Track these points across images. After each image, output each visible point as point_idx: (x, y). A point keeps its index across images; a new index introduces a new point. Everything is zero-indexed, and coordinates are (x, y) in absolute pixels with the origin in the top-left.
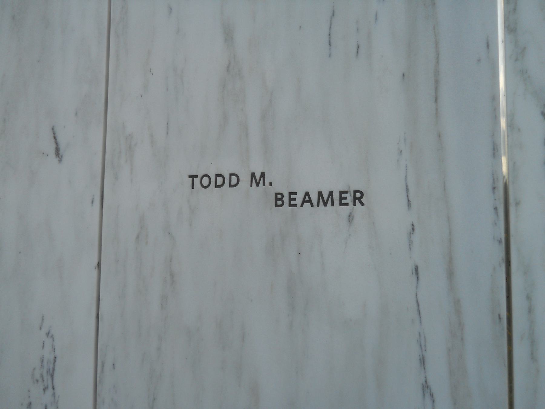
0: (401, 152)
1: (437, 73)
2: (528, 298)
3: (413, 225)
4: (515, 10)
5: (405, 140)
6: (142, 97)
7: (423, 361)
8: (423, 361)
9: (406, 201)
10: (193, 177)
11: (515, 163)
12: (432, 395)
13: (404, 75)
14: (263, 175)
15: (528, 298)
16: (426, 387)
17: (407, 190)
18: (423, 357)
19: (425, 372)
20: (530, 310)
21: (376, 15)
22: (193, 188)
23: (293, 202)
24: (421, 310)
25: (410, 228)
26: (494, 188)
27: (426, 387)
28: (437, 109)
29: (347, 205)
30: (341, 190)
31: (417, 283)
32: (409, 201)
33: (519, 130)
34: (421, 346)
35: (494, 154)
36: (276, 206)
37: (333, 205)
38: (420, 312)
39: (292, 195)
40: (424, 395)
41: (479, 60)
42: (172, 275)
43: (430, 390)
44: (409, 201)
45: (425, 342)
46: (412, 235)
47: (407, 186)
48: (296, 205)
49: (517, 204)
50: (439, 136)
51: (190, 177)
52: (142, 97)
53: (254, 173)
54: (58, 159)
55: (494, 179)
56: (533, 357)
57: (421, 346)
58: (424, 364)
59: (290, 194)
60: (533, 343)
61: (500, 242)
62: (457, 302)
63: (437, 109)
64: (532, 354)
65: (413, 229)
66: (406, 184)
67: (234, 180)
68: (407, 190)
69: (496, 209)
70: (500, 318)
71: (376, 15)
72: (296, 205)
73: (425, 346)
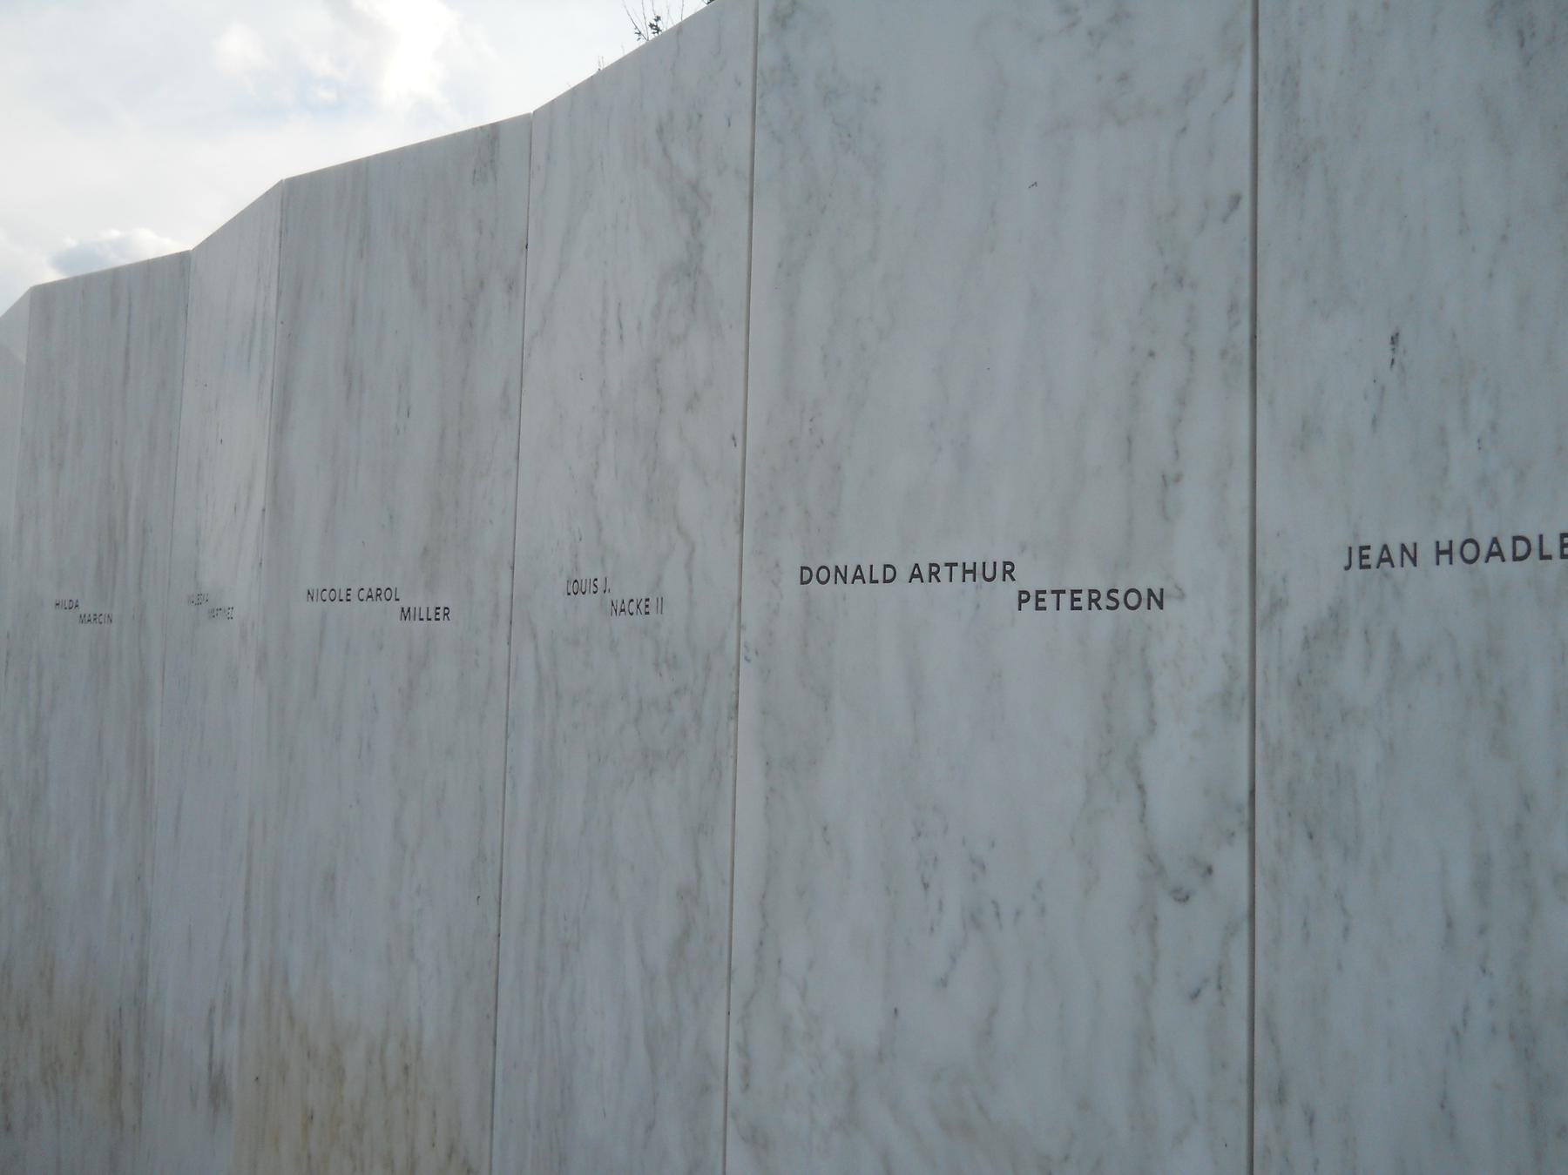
5: (639, 328)
6: (896, 1011)
23: (1365, 562)
29: (1080, 608)
36: (1072, 591)
48: (1369, 567)
52: (896, 1011)
54: (1391, 346)
59: (1362, 548)
67: (890, 572)
72: (1369, 567)
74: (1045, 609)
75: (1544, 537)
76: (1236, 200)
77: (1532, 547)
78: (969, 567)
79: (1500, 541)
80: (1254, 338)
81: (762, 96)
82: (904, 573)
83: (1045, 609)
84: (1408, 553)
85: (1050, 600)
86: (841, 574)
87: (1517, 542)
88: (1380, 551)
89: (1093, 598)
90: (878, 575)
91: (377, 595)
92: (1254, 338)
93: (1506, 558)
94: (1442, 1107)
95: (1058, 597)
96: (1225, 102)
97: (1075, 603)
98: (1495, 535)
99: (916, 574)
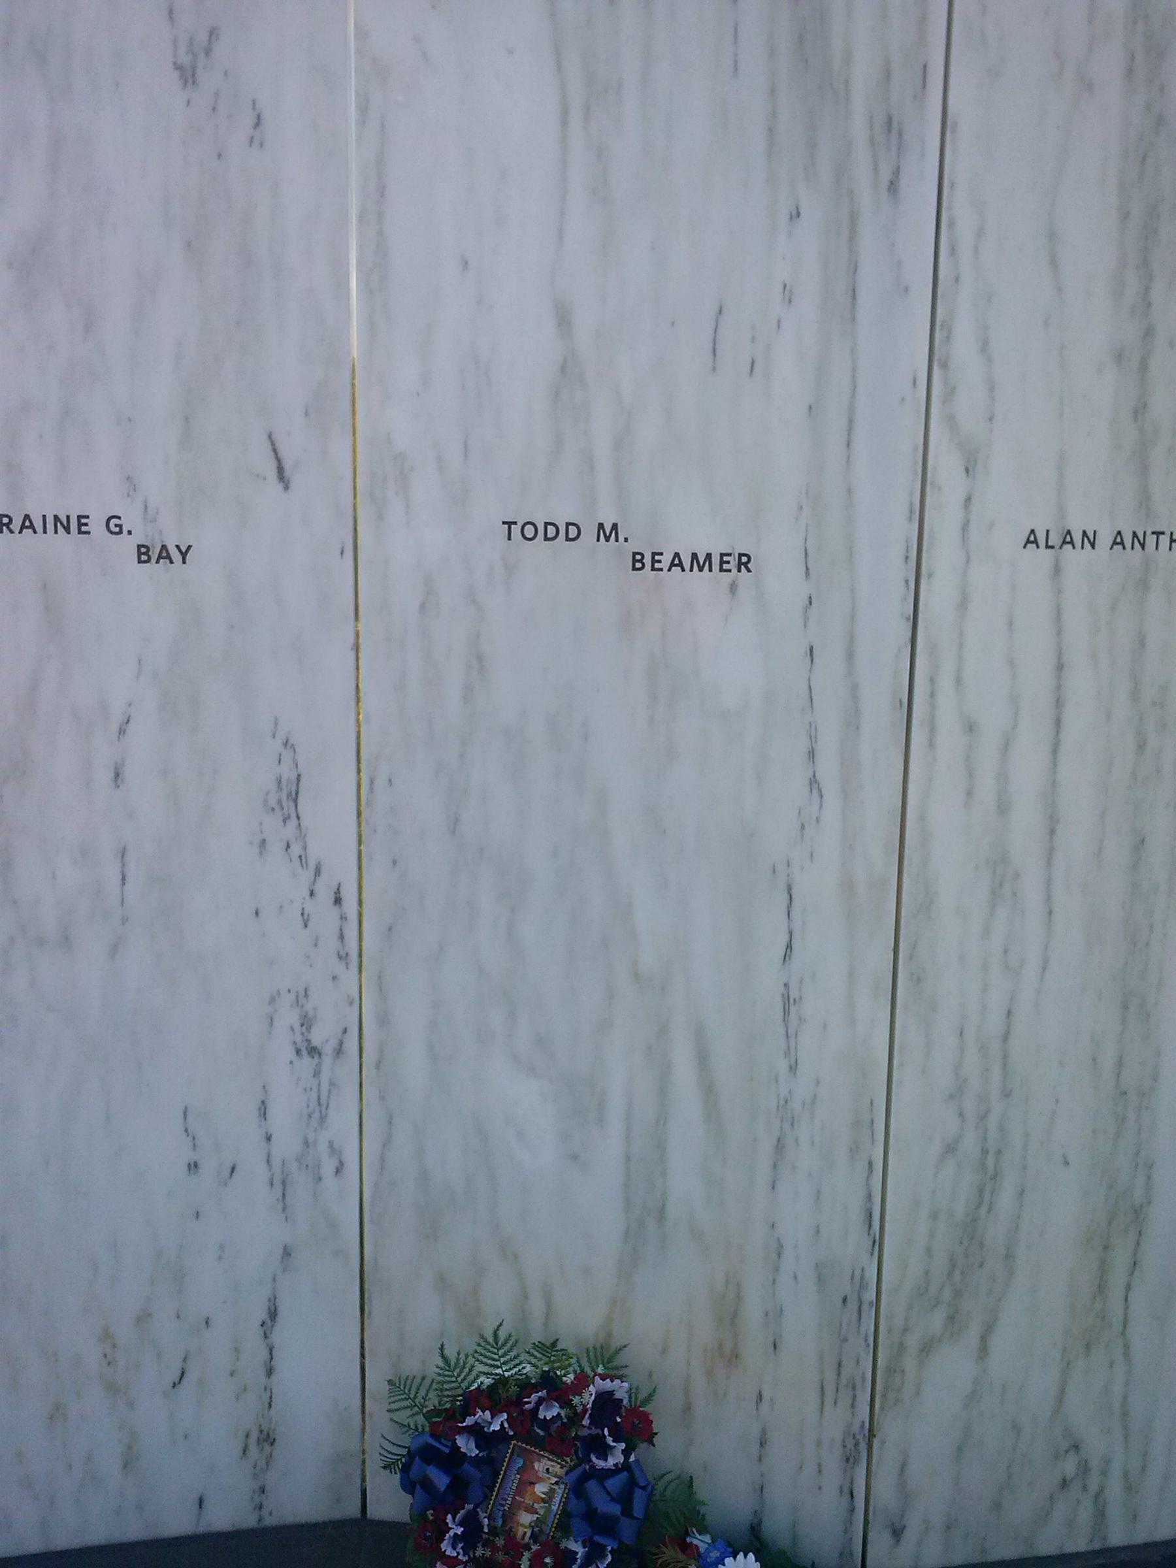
1: (851, 409)
2: (932, 681)
10: (510, 524)
12: (820, 790)
14: (615, 527)
15: (932, 681)
16: (814, 782)
20: (932, 695)
22: (1048, 531)
27: (814, 782)
32: (807, 568)
34: (811, 737)
37: (710, 570)
42: (480, 659)
44: (807, 568)
49: (930, 576)
51: (504, 523)
53: (711, 554)
56: (931, 744)
57: (811, 737)
60: (932, 730)
65: (810, 603)
67: (573, 531)
74: (88, 533)
75: (71, 517)
77: (561, 532)
79: (1122, 533)
82: (1105, 540)
83: (88, 533)
84: (61, 523)
85: (1151, 540)
86: (1088, 539)
88: (1028, 533)
89: (743, 561)
90: (1054, 540)
93: (37, 530)
94: (453, 832)
95: (1057, 570)
98: (1033, 528)
99: (1118, 541)
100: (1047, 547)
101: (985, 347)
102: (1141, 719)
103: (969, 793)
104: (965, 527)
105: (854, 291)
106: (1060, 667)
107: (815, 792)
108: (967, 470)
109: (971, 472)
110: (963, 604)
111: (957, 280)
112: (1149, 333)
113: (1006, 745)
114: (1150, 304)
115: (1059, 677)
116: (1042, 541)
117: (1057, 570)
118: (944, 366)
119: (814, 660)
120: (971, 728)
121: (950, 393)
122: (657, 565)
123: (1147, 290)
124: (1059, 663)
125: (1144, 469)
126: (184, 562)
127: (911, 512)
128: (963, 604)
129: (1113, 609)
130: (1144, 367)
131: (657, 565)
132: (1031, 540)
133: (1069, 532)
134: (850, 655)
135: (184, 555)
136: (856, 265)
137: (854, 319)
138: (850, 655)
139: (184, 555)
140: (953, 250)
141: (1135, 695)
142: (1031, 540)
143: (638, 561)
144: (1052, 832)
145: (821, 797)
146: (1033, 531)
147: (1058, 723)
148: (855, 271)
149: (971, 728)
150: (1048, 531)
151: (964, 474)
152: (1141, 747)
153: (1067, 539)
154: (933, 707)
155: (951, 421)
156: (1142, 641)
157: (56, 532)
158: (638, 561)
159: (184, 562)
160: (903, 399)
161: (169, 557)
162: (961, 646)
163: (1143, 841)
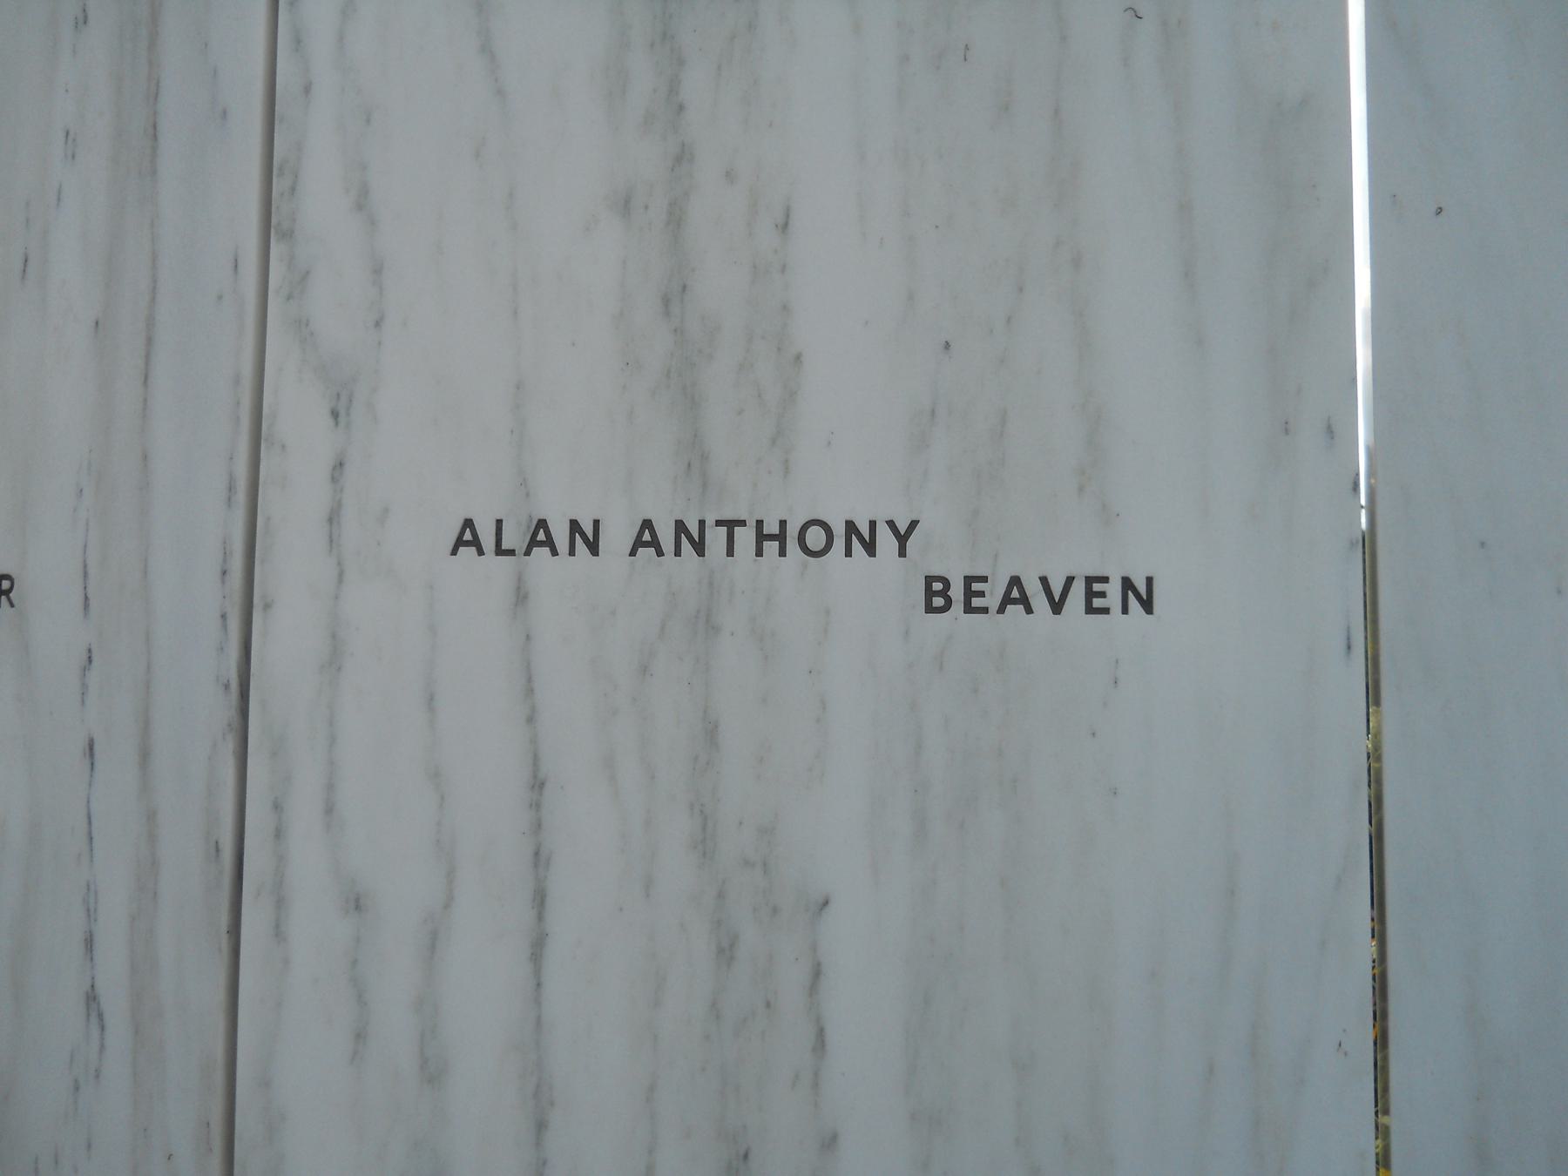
0: (81, 491)
1: (150, 322)
2: (277, 807)
3: (90, 651)
4: (293, 189)
7: (89, 943)
8: (89, 943)
9: (81, 599)
11: (269, 519)
12: (100, 1016)
13: (97, 323)
15: (277, 807)
16: (91, 998)
17: (86, 575)
18: (91, 935)
19: (92, 968)
20: (279, 834)
21: (59, 192)
22: (499, 522)
24: (95, 834)
25: (85, 656)
26: (224, 573)
27: (91, 998)
28: (145, 400)
30: (1091, 575)
31: (91, 776)
32: (86, 598)
33: (283, 447)
34: (88, 910)
35: (229, 499)
38: (91, 838)
39: (1094, 585)
40: (88, 1015)
41: (220, 298)
43: (99, 1004)
44: (86, 598)
45: (96, 903)
46: (87, 672)
47: (85, 566)
49: (267, 606)
50: (145, 458)
55: (225, 553)
56: (279, 932)
57: (88, 910)
58: (91, 951)
60: (280, 903)
61: (227, 686)
62: (151, 816)
63: (145, 400)
64: (277, 926)
65: (90, 660)
66: (85, 561)
68: (86, 575)
69: (224, 616)
70: (218, 850)
71: (59, 192)
73: (95, 910)
76: (1357, 542)
78: (772, 528)
80: (1368, 721)
81: (1357, 542)
82: (617, 537)
87: (1094, 606)
90: (514, 537)
91: (862, 538)
92: (1368, 721)
95: (521, 596)
96: (1349, 628)
97: (1095, 600)
98: (647, 517)
99: (645, 538)
100: (499, 551)
101: (362, 202)
102: (721, 895)
103: (360, 1036)
104: (333, 517)
105: (155, 126)
106: (538, 785)
107: (94, 1019)
108: (335, 414)
109: (342, 419)
110: (334, 660)
111: (307, 89)
112: (682, 157)
113: (433, 941)
114: (681, 108)
115: (536, 806)
116: (488, 540)
117: (521, 596)
118: (288, 235)
119: (96, 764)
120: (356, 904)
121: (301, 280)
122: (976, 602)
123: (673, 87)
124: (535, 777)
125: (690, 401)
126: (902, 553)
127: (231, 488)
128: (334, 660)
129: (644, 670)
130: (676, 219)
131: (976, 602)
132: (467, 537)
133: (542, 524)
134: (145, 755)
135: (902, 539)
136: (158, 85)
137: (154, 172)
138: (145, 755)
139: (902, 539)
140: (298, 41)
141: (704, 844)
142: (467, 537)
143: (938, 594)
144: (541, 1126)
145: (103, 1028)
146: (468, 523)
147: (540, 899)
148: (156, 98)
149: (356, 904)
150: (499, 522)
151: (331, 422)
152: (726, 952)
153: (540, 535)
154: (281, 859)
155: (302, 328)
156: (711, 733)
157: (848, 553)
158: (938, 594)
159: (902, 553)
160: (220, 298)
161: (1024, 601)
162: (332, 740)
163: (746, 1156)
